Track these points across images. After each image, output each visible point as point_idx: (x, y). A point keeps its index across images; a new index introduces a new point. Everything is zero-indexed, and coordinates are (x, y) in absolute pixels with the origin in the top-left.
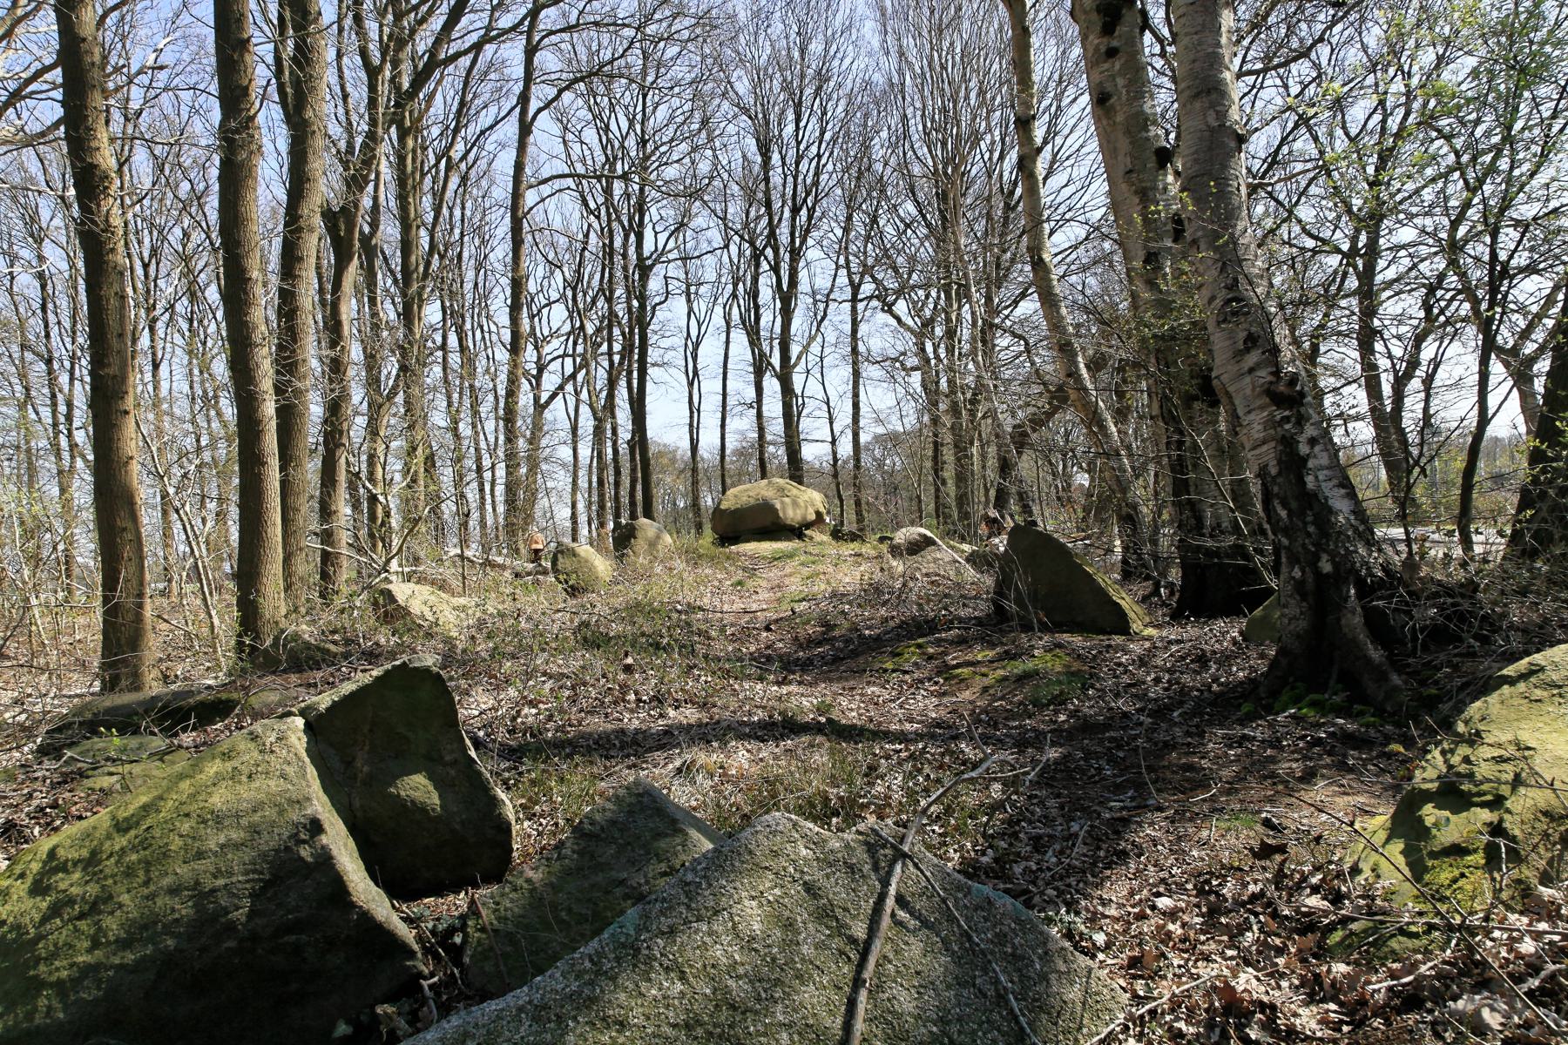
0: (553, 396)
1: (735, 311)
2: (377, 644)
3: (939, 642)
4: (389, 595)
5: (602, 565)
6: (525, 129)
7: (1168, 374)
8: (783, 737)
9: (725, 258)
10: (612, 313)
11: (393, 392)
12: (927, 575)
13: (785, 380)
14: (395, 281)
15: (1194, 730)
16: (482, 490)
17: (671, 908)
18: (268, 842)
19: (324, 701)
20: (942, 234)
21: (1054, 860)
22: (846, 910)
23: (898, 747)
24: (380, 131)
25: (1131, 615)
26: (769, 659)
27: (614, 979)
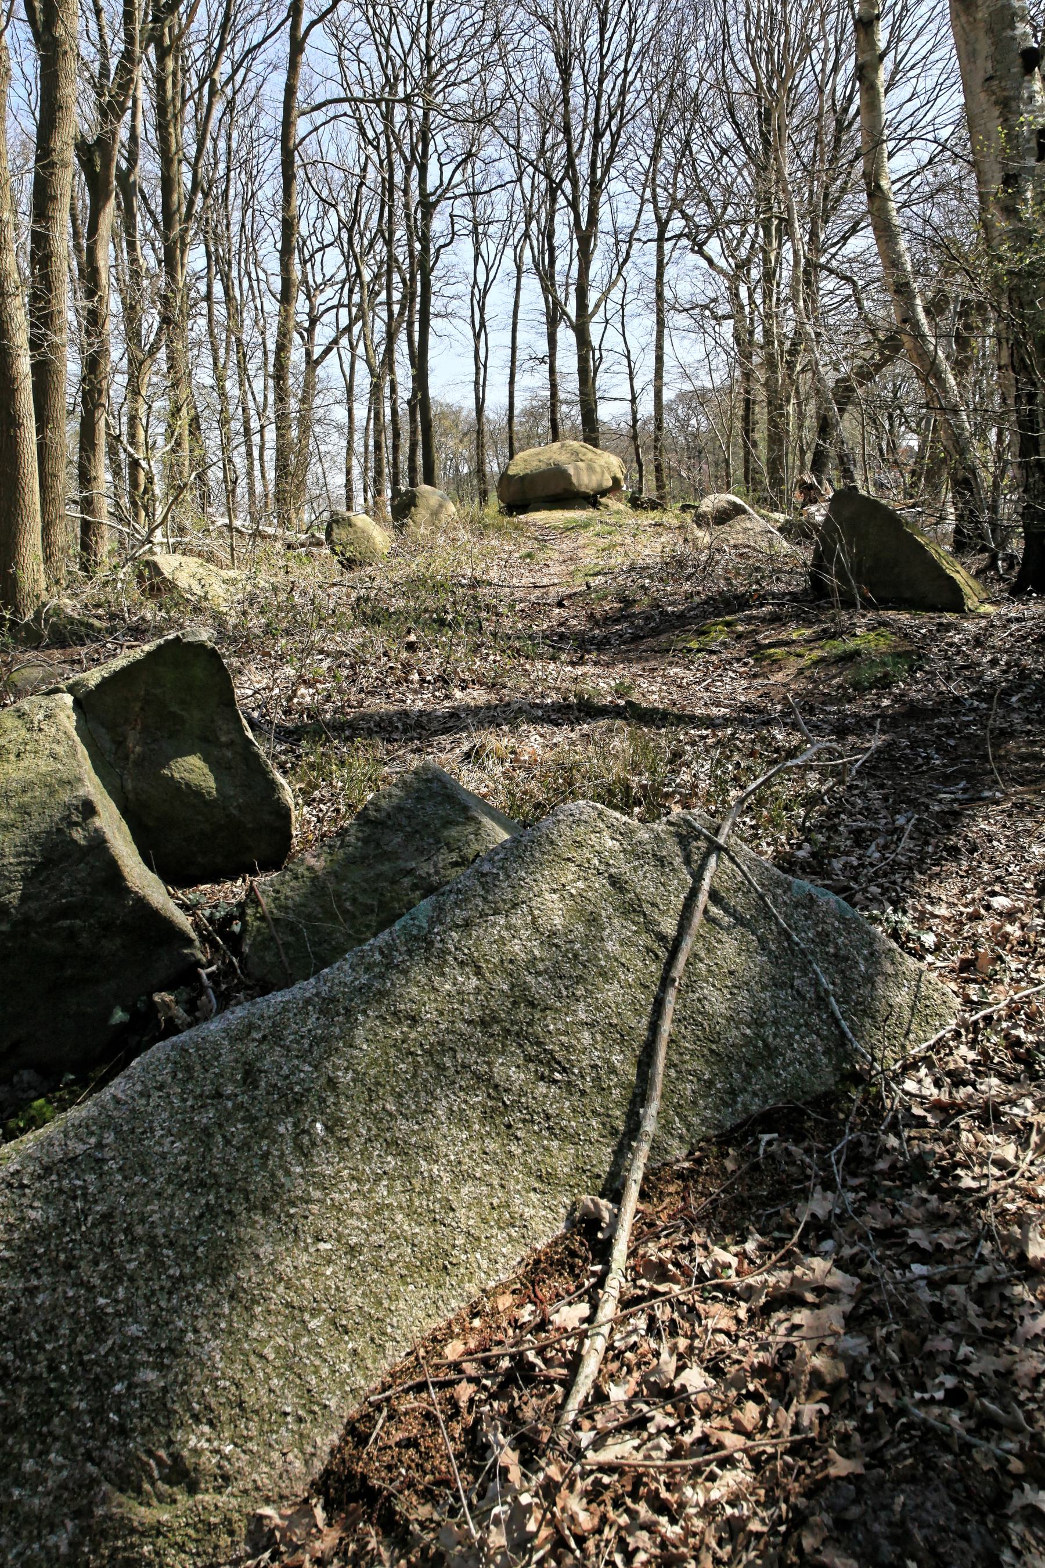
0: (327, 351)
1: (527, 254)
2: (143, 619)
3: (749, 619)
4: (154, 567)
5: (381, 537)
6: (297, 46)
7: (1022, 316)
8: (578, 721)
9: (518, 194)
10: (392, 258)
11: (154, 349)
12: (735, 546)
13: (581, 332)
14: (156, 224)
15: (1034, 716)
16: (249, 454)
17: (466, 900)
18: (38, 824)
19: (94, 677)
20: (763, 162)
21: (877, 855)
22: (654, 905)
23: (704, 732)
24: (137, 50)
25: (966, 590)
26: (562, 637)
27: (405, 972)
